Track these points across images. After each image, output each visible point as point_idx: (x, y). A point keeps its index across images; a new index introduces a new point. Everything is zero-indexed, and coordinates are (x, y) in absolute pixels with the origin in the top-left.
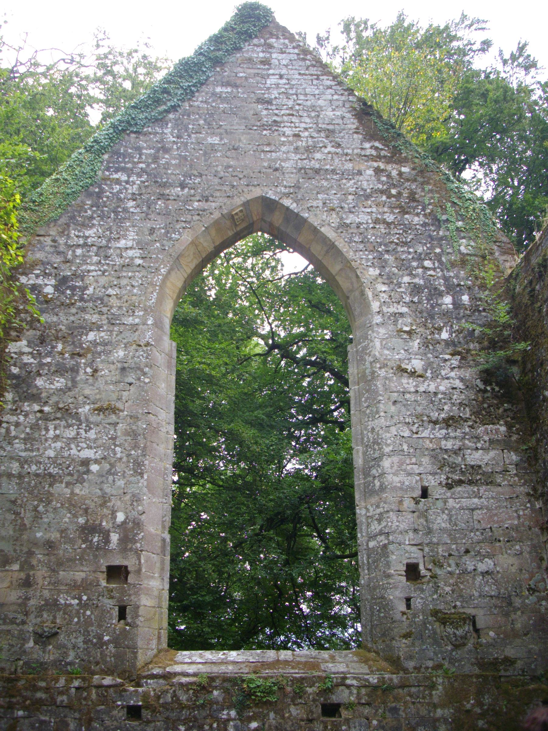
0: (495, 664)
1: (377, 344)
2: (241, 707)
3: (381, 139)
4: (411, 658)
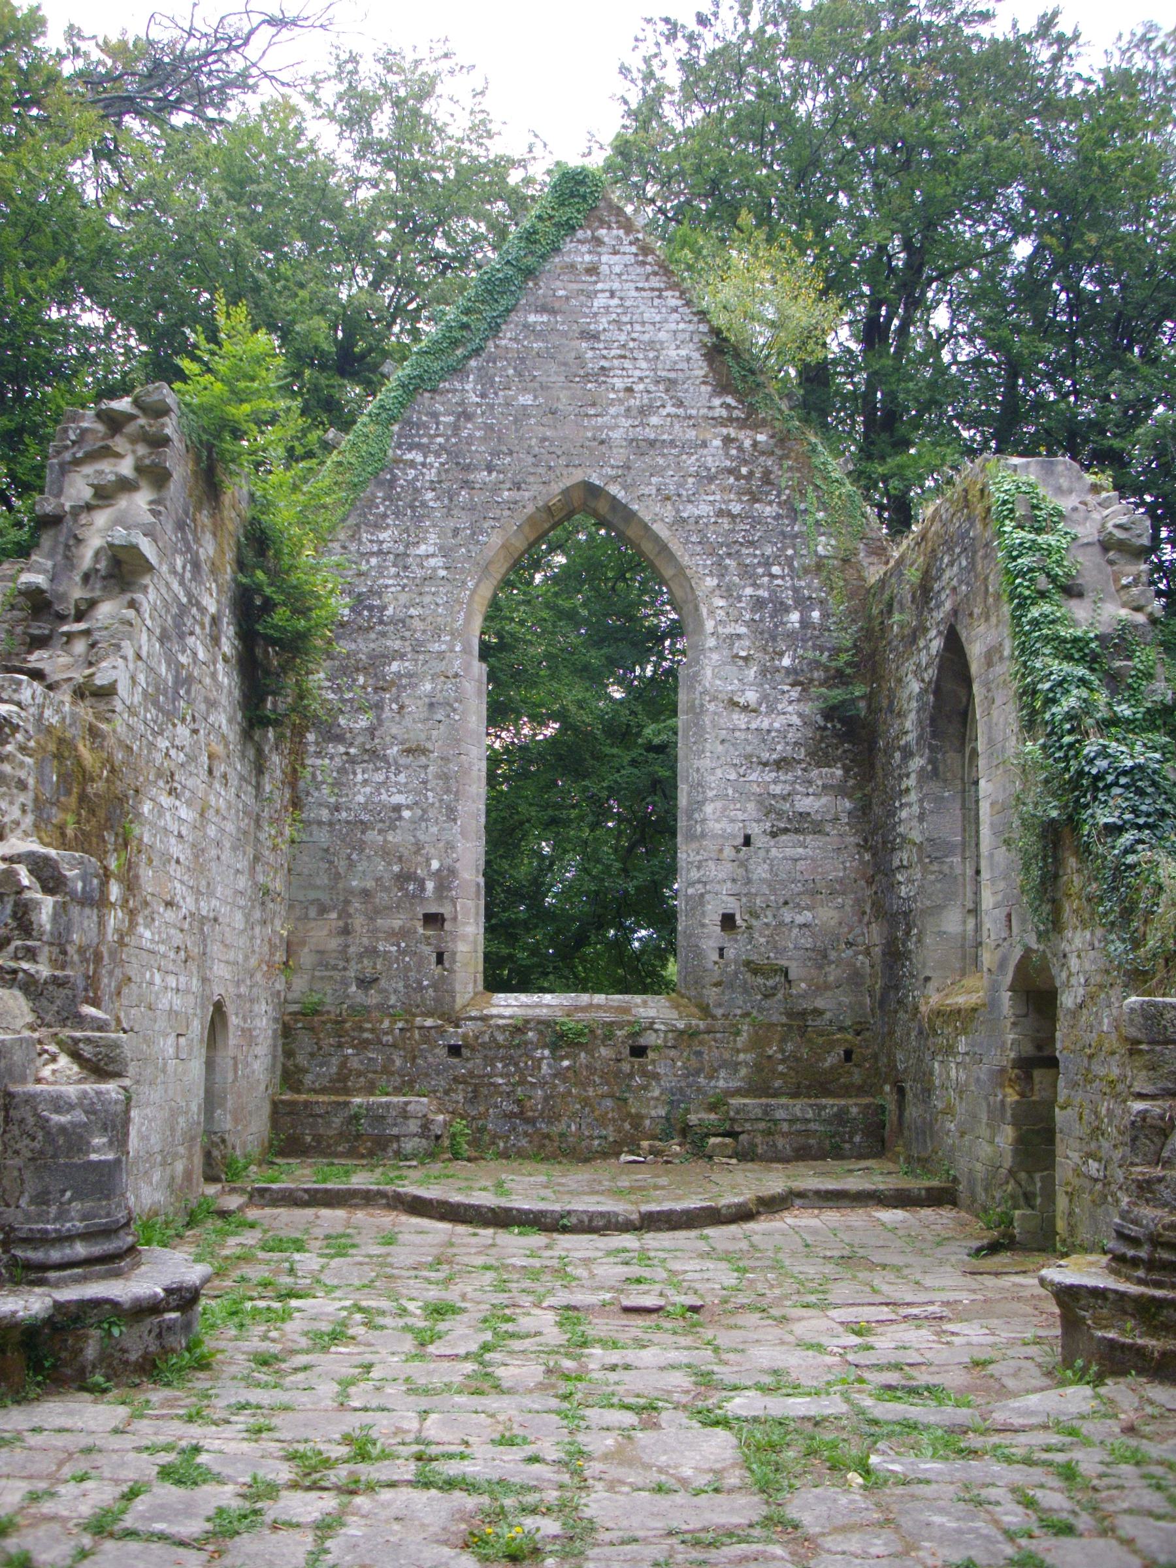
0: (803, 1014)
1: (709, 672)
2: (554, 1047)
3: (734, 392)
4: (720, 1005)
